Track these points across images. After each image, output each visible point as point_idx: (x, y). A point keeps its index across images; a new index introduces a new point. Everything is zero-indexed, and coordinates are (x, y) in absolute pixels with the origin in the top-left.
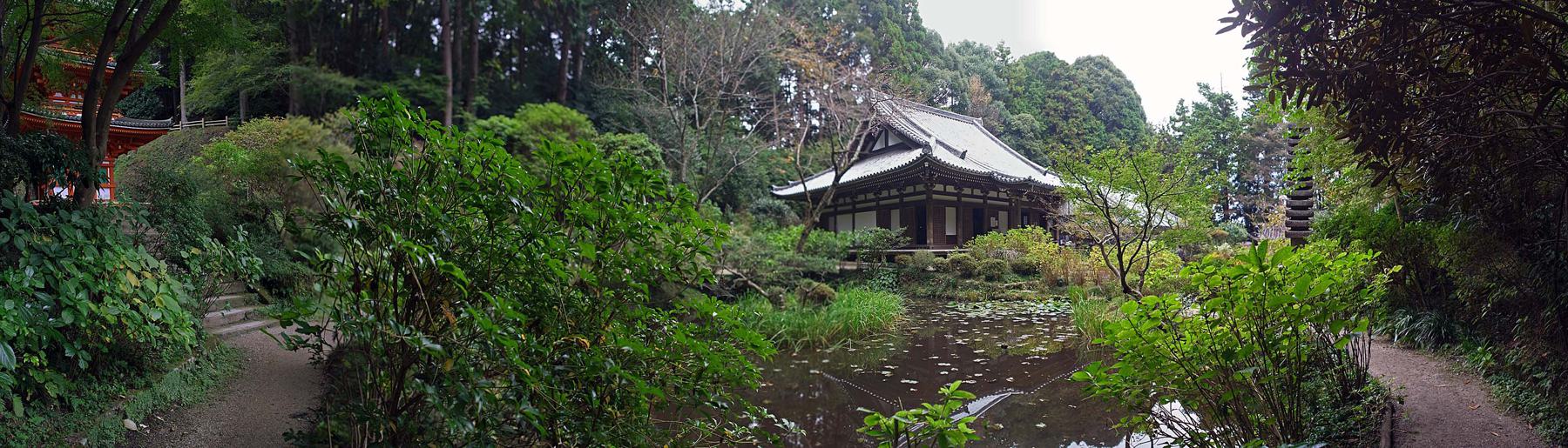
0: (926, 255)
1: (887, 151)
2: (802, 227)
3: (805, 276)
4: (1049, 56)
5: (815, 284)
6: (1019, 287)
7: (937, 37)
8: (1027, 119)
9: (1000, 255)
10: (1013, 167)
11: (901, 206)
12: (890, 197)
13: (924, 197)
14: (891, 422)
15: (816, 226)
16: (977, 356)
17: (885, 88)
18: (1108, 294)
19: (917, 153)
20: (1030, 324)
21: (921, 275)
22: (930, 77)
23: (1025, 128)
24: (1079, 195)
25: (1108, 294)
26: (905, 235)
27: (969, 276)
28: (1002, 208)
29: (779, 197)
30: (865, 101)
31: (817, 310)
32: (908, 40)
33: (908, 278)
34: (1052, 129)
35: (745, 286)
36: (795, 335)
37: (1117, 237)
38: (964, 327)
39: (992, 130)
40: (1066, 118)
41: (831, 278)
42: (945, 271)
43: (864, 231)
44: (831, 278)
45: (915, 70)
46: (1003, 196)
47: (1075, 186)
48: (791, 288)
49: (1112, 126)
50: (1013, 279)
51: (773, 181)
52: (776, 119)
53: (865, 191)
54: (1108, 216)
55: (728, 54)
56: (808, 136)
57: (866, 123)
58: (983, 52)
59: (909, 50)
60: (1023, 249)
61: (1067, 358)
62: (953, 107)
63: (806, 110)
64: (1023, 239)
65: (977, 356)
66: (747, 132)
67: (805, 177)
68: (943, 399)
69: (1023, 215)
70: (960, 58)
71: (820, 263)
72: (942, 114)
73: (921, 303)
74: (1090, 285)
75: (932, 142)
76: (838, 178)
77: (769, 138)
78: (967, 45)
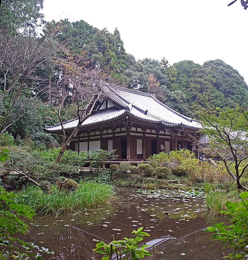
0: (126, 164)
1: (107, 110)
2: (60, 148)
3: (61, 174)
4: (190, 63)
5: (66, 179)
6: (176, 182)
7: (133, 57)
8: (178, 93)
9: (166, 165)
10: (173, 118)
11: (113, 138)
12: (108, 134)
13: (125, 134)
14: (109, 246)
15: (68, 148)
16: (152, 218)
17: (107, 80)
18: (227, 189)
19: (122, 112)
20: (181, 202)
21: (124, 175)
22: (129, 75)
23: (178, 98)
24: (212, 133)
25: (227, 189)
26: (115, 154)
27: (149, 176)
28: (167, 140)
29: (48, 132)
30: (97, 86)
31: (67, 194)
32: (118, 58)
33: (117, 176)
34: (194, 98)
35: (27, 180)
36: (56, 207)
37: (235, 157)
38: (146, 203)
39: (160, 100)
40: (201, 92)
41: (75, 176)
42: (136, 173)
43: (93, 151)
44: (75, 176)
45: (122, 72)
46: (167, 133)
47: (210, 128)
48: (53, 182)
49: (227, 94)
50: (173, 178)
51: (45, 122)
52: (50, 91)
53: (95, 130)
54: (229, 144)
55: (28, 57)
56: (66, 101)
57: (97, 96)
58: (155, 63)
59: (119, 63)
60: (179, 162)
61: (199, 222)
62: (140, 89)
63: (67, 89)
64: (178, 156)
65: (152, 218)
66: (33, 96)
67: (63, 121)
68: (134, 236)
69: (178, 143)
70: (144, 66)
71: (69, 168)
72: (135, 92)
73: (123, 190)
74: (216, 183)
75: (130, 106)
76: (80, 123)
77: (45, 100)
78: (147, 60)
